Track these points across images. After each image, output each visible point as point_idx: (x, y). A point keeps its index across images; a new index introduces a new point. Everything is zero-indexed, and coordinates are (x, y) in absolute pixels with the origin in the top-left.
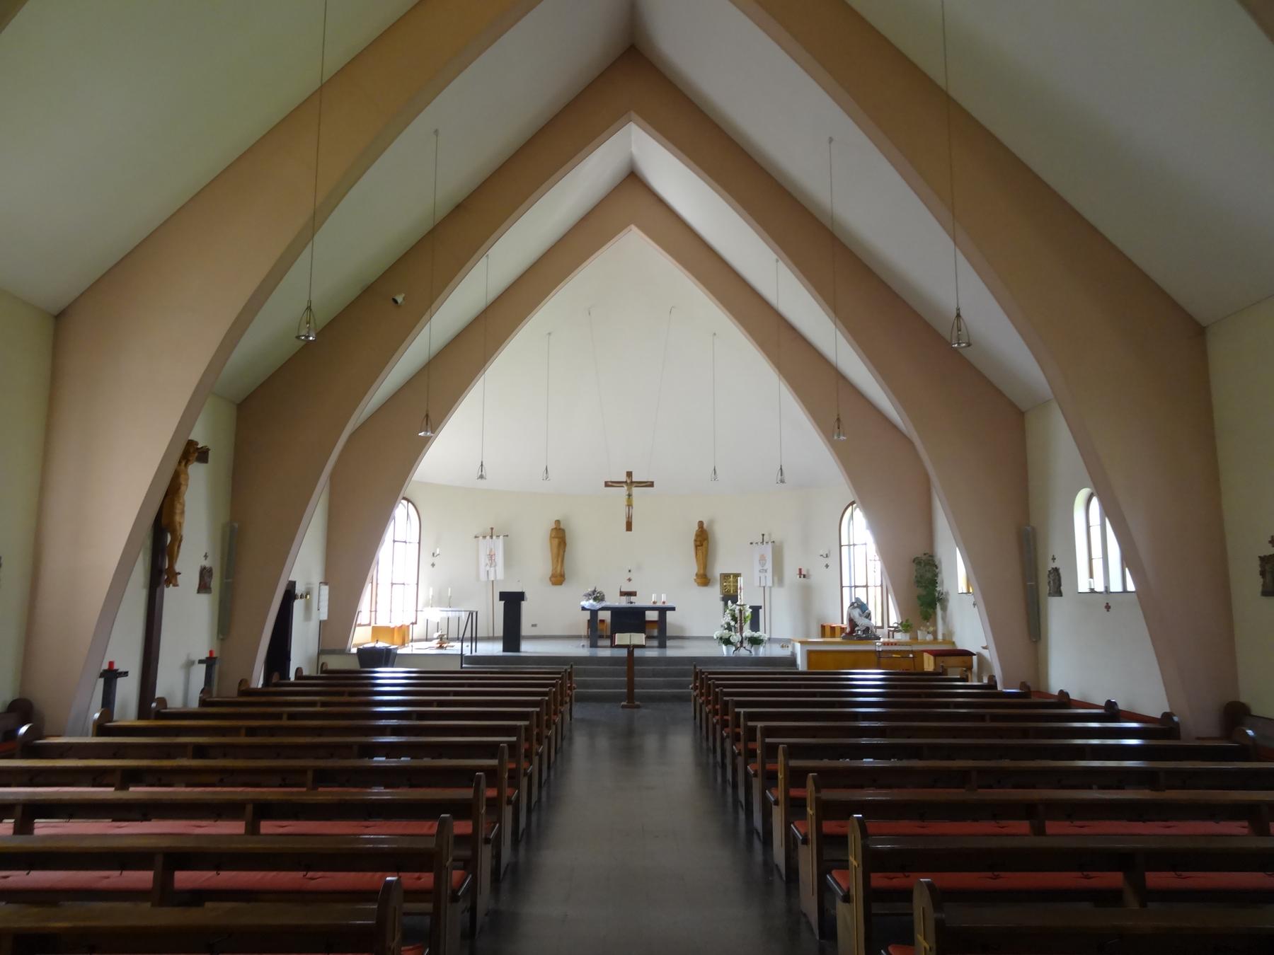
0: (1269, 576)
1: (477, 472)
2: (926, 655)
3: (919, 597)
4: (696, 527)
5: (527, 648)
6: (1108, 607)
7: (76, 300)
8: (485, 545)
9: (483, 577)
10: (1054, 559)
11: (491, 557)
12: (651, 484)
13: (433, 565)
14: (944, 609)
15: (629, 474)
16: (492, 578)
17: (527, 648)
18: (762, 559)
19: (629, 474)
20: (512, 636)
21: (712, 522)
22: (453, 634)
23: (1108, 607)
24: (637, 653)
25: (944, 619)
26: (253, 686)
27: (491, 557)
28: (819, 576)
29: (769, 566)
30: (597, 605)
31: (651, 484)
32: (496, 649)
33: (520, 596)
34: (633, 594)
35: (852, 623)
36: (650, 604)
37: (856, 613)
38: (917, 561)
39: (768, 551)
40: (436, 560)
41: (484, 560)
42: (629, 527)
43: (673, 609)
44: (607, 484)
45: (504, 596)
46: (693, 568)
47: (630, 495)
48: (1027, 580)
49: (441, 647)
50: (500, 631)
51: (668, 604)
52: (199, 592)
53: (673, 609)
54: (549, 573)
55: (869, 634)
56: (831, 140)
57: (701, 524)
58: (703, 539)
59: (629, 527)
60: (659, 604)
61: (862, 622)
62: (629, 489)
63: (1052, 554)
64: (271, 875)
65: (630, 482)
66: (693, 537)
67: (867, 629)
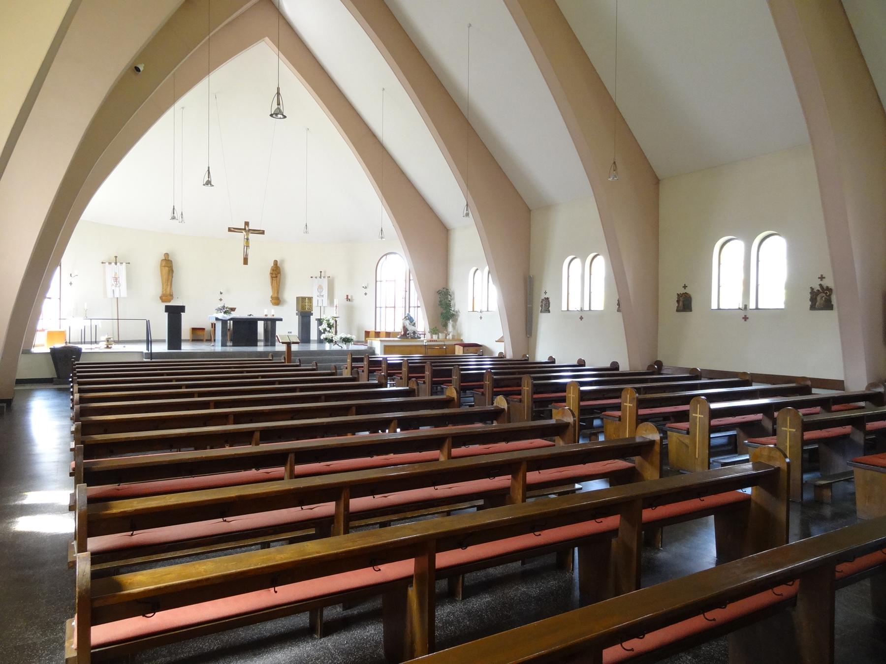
0: (681, 303)
1: (170, 215)
2: (457, 347)
3: (442, 314)
4: (810, 291)
5: (186, 348)
6: (581, 318)
7: (658, 194)
8: (111, 270)
9: (110, 295)
10: (546, 293)
11: (116, 279)
12: (263, 232)
13: (71, 284)
14: (455, 321)
15: (247, 224)
16: (117, 295)
17: (186, 348)
18: (320, 288)
19: (247, 224)
20: (175, 337)
21: (283, 261)
22: (88, 339)
23: (581, 318)
24: (294, 348)
25: (454, 327)
26: (457, 354)
27: (116, 279)
28: (359, 299)
29: (325, 292)
30: (227, 317)
31: (263, 232)
32: (161, 348)
33: (182, 309)
34: (233, 309)
35: (405, 329)
36: (263, 316)
37: (408, 322)
38: (439, 292)
39: (325, 283)
40: (73, 280)
41: (110, 281)
42: (246, 261)
43: (281, 320)
44: (230, 230)
45: (168, 309)
46: (269, 292)
47: (247, 239)
48: (527, 302)
49: (108, 347)
50: (165, 336)
51: (276, 317)
52: (691, 310)
53: (281, 320)
54: (160, 293)
55: (415, 336)
56: (470, 25)
57: (276, 262)
58: (276, 272)
59: (246, 261)
60: (269, 317)
61: (411, 328)
62: (247, 235)
63: (547, 289)
64: (369, 459)
65: (246, 229)
66: (269, 270)
67: (414, 333)
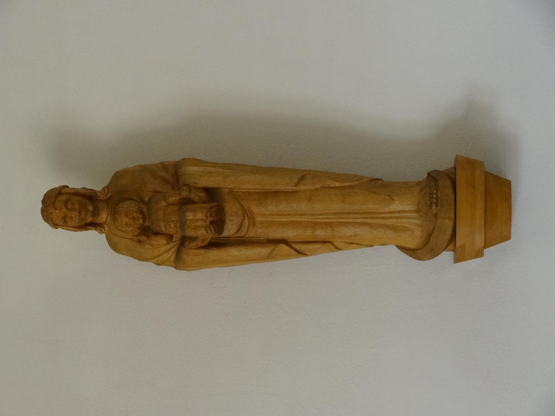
42: (171, 203)
46: (371, 279)
57: (67, 208)
59: (171, 203)
